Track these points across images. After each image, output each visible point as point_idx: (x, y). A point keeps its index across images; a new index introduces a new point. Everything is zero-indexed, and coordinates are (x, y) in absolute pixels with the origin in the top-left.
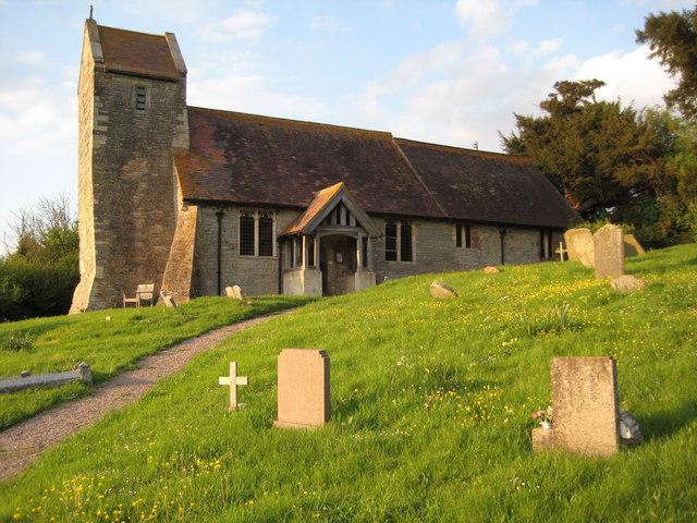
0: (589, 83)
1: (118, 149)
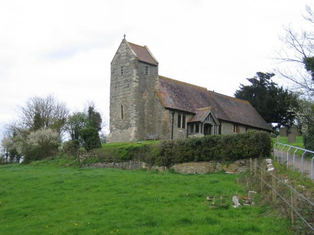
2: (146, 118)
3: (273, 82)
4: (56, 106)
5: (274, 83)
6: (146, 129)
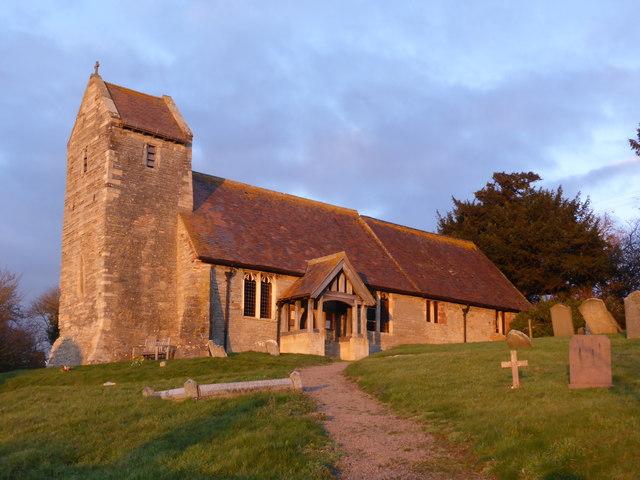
0: (523, 175)
1: (130, 201)
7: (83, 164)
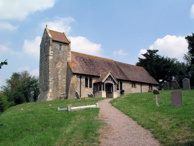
1: (55, 59)
2: (59, 82)
3: (158, 55)
4: (11, 79)
5: (158, 56)
6: (60, 90)
7: (44, 50)
